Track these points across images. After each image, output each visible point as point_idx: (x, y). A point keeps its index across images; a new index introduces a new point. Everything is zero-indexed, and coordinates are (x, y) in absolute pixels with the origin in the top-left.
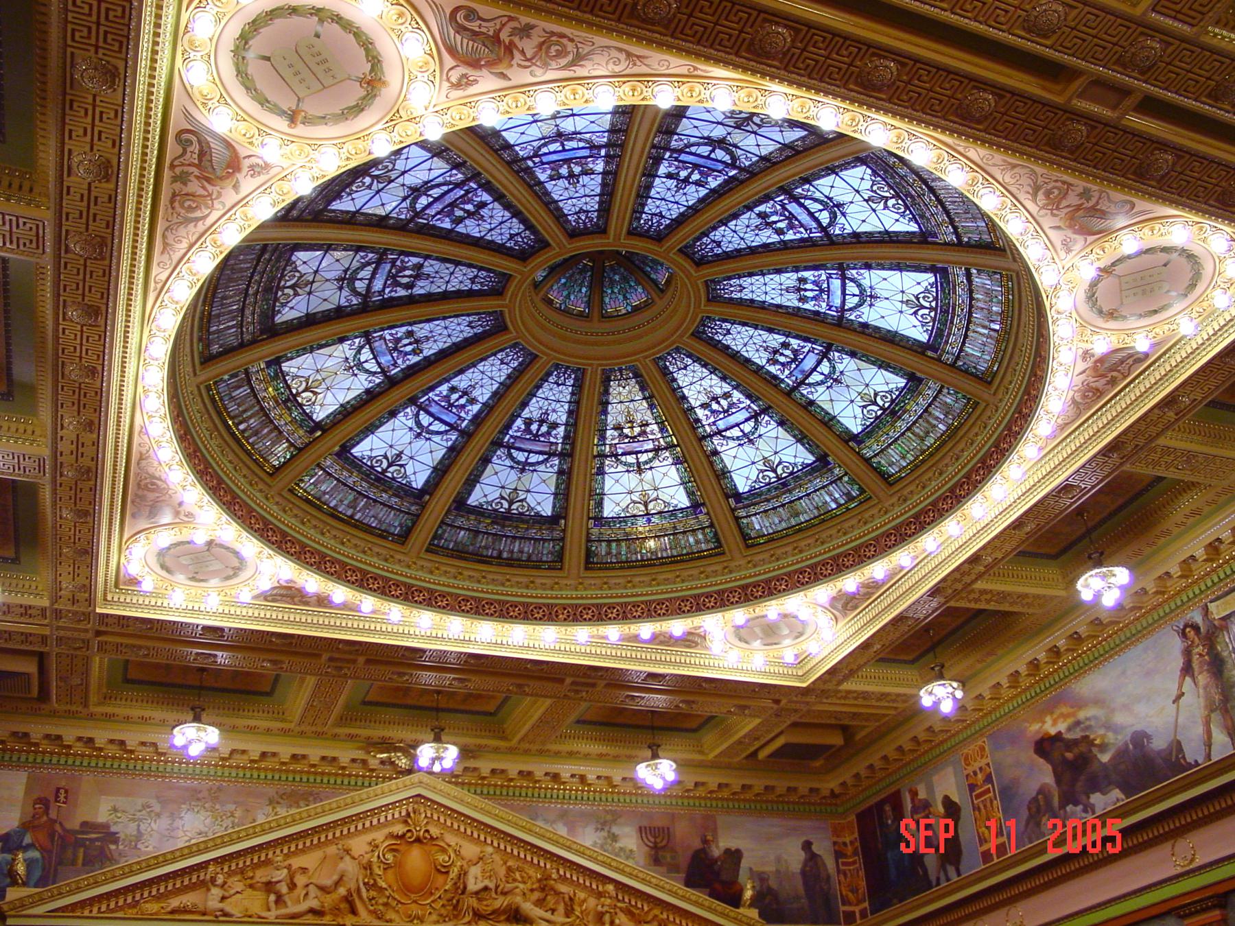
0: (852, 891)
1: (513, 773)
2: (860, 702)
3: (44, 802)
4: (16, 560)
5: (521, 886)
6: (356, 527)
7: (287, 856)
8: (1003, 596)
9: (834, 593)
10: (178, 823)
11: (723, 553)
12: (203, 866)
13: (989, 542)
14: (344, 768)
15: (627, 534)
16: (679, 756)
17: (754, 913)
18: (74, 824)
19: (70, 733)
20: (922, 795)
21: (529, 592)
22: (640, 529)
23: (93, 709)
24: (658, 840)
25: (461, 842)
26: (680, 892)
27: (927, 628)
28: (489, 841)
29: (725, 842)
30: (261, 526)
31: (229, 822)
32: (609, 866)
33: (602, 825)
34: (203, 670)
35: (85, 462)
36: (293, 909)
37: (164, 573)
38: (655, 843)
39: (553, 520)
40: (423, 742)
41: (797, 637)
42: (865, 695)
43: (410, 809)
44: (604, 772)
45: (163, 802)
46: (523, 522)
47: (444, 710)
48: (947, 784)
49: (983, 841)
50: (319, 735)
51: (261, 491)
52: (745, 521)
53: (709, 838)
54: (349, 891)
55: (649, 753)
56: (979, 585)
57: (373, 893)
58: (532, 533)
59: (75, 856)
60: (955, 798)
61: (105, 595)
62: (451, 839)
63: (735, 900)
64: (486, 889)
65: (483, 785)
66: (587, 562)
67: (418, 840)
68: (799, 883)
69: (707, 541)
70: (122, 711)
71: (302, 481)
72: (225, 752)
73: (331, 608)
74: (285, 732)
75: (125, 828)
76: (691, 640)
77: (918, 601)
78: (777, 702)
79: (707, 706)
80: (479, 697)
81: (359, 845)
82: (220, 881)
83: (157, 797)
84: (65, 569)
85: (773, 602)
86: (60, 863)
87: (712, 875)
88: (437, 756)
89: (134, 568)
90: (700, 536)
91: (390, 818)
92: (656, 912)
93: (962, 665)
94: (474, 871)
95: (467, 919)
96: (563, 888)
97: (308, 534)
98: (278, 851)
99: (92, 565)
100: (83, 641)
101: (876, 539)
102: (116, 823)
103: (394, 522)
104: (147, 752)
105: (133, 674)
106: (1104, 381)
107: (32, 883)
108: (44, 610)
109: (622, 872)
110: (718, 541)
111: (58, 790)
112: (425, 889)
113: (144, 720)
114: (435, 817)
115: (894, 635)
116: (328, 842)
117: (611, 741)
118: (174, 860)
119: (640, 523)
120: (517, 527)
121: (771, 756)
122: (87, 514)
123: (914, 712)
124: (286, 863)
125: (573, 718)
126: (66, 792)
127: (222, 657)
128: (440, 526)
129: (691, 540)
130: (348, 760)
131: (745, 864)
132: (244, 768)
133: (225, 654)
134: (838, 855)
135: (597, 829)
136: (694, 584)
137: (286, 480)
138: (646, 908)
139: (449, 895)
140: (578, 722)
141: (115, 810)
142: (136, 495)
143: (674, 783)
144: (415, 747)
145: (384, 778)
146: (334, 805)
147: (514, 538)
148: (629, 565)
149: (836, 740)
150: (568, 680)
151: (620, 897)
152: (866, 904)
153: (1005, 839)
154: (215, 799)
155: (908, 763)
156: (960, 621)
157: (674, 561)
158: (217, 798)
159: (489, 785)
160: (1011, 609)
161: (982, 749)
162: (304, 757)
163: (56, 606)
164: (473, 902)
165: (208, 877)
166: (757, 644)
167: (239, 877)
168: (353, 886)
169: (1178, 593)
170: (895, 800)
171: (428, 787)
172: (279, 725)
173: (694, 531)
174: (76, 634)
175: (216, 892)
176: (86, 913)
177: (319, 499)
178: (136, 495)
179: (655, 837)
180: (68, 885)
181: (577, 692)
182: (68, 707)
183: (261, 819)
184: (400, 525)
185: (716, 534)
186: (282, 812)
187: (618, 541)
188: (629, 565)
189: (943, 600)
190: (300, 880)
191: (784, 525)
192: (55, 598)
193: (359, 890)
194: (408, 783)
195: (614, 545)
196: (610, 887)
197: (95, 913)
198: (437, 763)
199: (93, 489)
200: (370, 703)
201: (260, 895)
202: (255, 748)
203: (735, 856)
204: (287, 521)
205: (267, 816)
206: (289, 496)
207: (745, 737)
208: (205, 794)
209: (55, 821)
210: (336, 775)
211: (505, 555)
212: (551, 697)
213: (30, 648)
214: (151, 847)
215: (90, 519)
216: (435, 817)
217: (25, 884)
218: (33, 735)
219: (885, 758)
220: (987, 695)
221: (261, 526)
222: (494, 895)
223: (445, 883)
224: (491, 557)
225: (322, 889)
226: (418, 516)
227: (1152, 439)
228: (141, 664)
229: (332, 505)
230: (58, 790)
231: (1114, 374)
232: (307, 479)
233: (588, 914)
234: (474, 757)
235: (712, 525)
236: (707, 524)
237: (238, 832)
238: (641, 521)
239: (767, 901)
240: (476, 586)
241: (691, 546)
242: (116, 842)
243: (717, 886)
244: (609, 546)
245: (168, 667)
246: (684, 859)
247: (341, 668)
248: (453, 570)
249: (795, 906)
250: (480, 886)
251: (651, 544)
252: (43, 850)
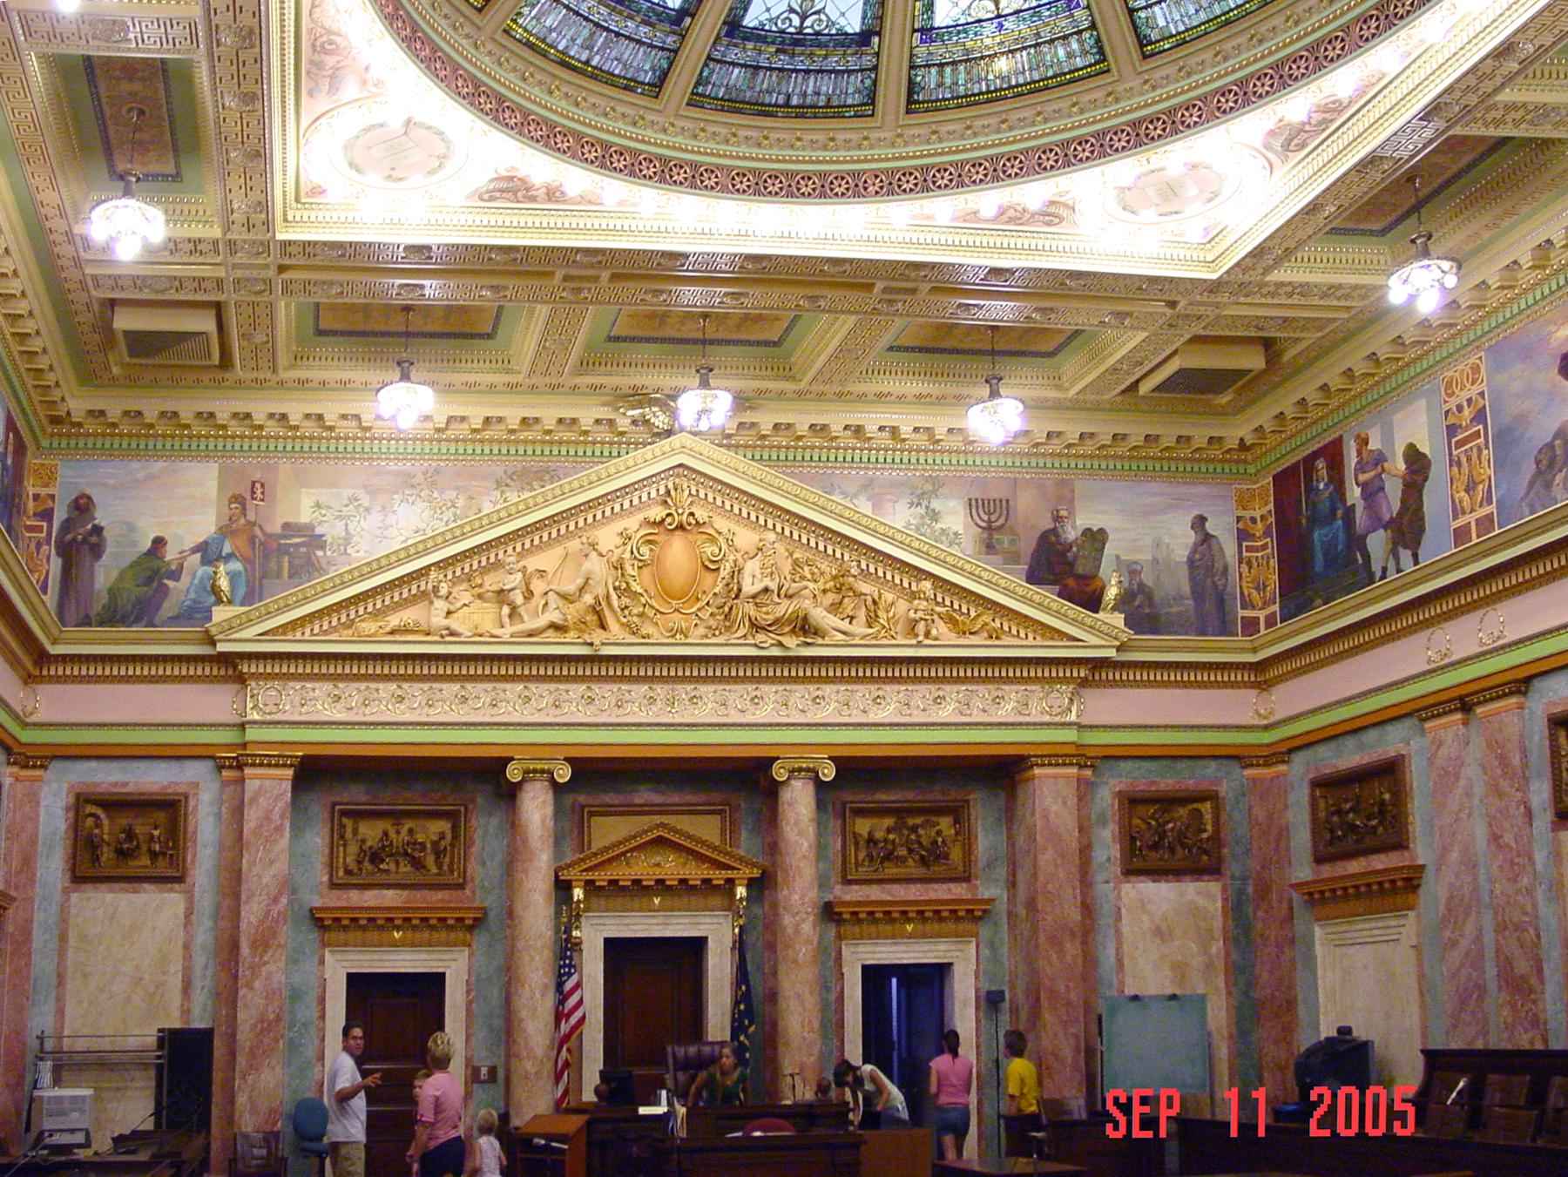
0: (1257, 589)
1: (802, 429)
2: (1295, 300)
3: (238, 499)
4: (177, 177)
5: (811, 585)
6: (593, 77)
7: (521, 556)
8: (1544, 112)
9: (1271, 124)
10: (391, 519)
11: (1108, 71)
12: (423, 573)
13: (1533, 19)
14: (586, 433)
15: (967, 51)
16: (1025, 393)
17: (1118, 620)
18: (275, 527)
19: (260, 409)
20: (1374, 444)
21: (828, 155)
22: (988, 42)
23: (284, 375)
24: (993, 518)
25: (735, 528)
26: (1020, 590)
27: (1410, 177)
28: (770, 526)
29: (1084, 519)
30: (471, 89)
31: (449, 515)
32: (926, 555)
33: (919, 498)
34: (407, 309)
35: (246, 19)
36: (531, 624)
37: (353, 173)
38: (989, 521)
39: (864, 38)
40: (685, 390)
41: (1210, 200)
42: (1303, 289)
43: (671, 486)
44: (922, 422)
45: (372, 492)
46: (820, 45)
47: (712, 342)
48: (1414, 427)
49: (1457, 512)
50: (554, 388)
51: (467, 36)
52: (1143, 14)
53: (1063, 513)
54: (596, 598)
55: (986, 391)
56: (1506, 96)
57: (625, 601)
58: (833, 62)
59: (280, 564)
60: (1424, 448)
61: (285, 215)
62: (722, 524)
63: (1092, 602)
64: (766, 590)
65: (763, 447)
66: (910, 101)
67: (681, 527)
68: (1184, 572)
69: (1084, 53)
70: (317, 375)
71: (519, 14)
72: (441, 421)
73: (564, 202)
74: (512, 388)
75: (331, 530)
76: (1051, 215)
77: (1402, 129)
78: (1172, 304)
79: (1073, 316)
80: (760, 318)
81: (607, 537)
82: (443, 592)
83: (365, 487)
84: (235, 182)
85: (1179, 144)
86: (264, 576)
87: (1062, 567)
88: (705, 406)
89: (315, 173)
90: (1075, 46)
91: (645, 498)
92: (986, 618)
93: (1455, 236)
94: (752, 567)
95: (741, 633)
96: (865, 588)
97: (535, 95)
98: (510, 549)
99: (266, 174)
100: (264, 281)
101: (1346, 28)
102: (320, 523)
103: (643, 64)
104: (350, 427)
105: (325, 324)
107: (238, 599)
108: (215, 242)
109: (943, 563)
110: (1101, 51)
111: (253, 483)
112: (689, 594)
113: (344, 384)
114: (702, 495)
115: (1358, 190)
116: (570, 535)
117: (931, 375)
118: (390, 566)
119: (986, 32)
120: (811, 55)
121: (1157, 389)
122: (254, 98)
123: (1373, 314)
124: (520, 565)
125: (887, 339)
126: (263, 486)
127: (432, 288)
128: (706, 65)
129: (1061, 53)
130: (591, 421)
131: (1109, 550)
132: (465, 441)
133: (435, 283)
134: (1243, 535)
135: (912, 504)
136: (1061, 123)
137: (500, 16)
138: (973, 614)
139: (720, 601)
140: (891, 349)
141: (318, 506)
142: (312, 62)
143: (1017, 435)
144: (674, 398)
145: (637, 444)
146: (575, 485)
147: (807, 72)
148: (969, 101)
149: (1254, 361)
150: (880, 285)
151: (939, 599)
152: (1276, 607)
153: (1493, 508)
154: (433, 485)
155: (1359, 396)
156: (1466, 159)
157: (1035, 88)
158: (434, 483)
159: (771, 447)
160: (1556, 135)
161: (1476, 369)
162: (537, 420)
163: (229, 236)
164: (750, 609)
165: (430, 586)
166: (1149, 215)
167: (464, 586)
168: (601, 591)
170: (1333, 453)
171: (692, 453)
172: (506, 378)
173: (1065, 37)
174: (255, 273)
175: (440, 605)
176: (298, 636)
177: (543, 41)
178: (312, 62)
179: (989, 514)
180: (275, 601)
181: (890, 302)
182: (255, 374)
183: (488, 508)
184: (653, 69)
185: (1098, 40)
186: (513, 497)
187: (954, 63)
188: (969, 101)
189: (1442, 125)
190: (538, 586)
191: (1203, 16)
192: (228, 226)
193: (608, 597)
194: (667, 448)
195: (948, 70)
196: (927, 585)
197: (307, 637)
198: (704, 417)
199: (259, 60)
200: (618, 339)
201: (491, 607)
202: (476, 412)
203: (1096, 538)
204: (503, 78)
205: (495, 504)
206: (504, 40)
207: (1120, 361)
208: (420, 478)
209: (254, 524)
210: (577, 443)
211: (795, 101)
212: (856, 312)
213: (206, 298)
214: (364, 550)
215: (258, 105)
216: (702, 495)
217: (230, 602)
218: (219, 415)
219: (1324, 388)
220: (1494, 282)
221: (471, 89)
222: (777, 600)
223: (715, 585)
224: (776, 105)
225: (563, 596)
226: (676, 52)
228: (334, 308)
229: (560, 47)
230: (253, 483)
232: (526, 10)
233: (896, 623)
234: (751, 408)
235: (1093, 26)
236: (1086, 24)
237: (461, 526)
238: (989, 28)
239: (1137, 603)
240: (754, 151)
241: (1060, 63)
242: (323, 547)
243: (1071, 582)
244: (941, 74)
245: (366, 309)
246: (1027, 546)
247: (580, 290)
248: (724, 131)
249: (1175, 610)
250: (758, 587)
251: (1003, 65)
252: (247, 561)
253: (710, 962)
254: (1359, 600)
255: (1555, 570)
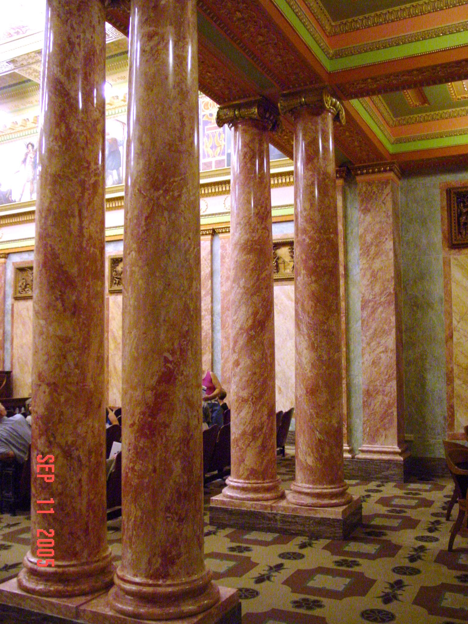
106: (14, 31)
169: (30, 129)
220: (20, 123)
227: (29, 64)
231: (19, 30)
253: (286, 287)
254: (280, 163)
255: (113, 207)
